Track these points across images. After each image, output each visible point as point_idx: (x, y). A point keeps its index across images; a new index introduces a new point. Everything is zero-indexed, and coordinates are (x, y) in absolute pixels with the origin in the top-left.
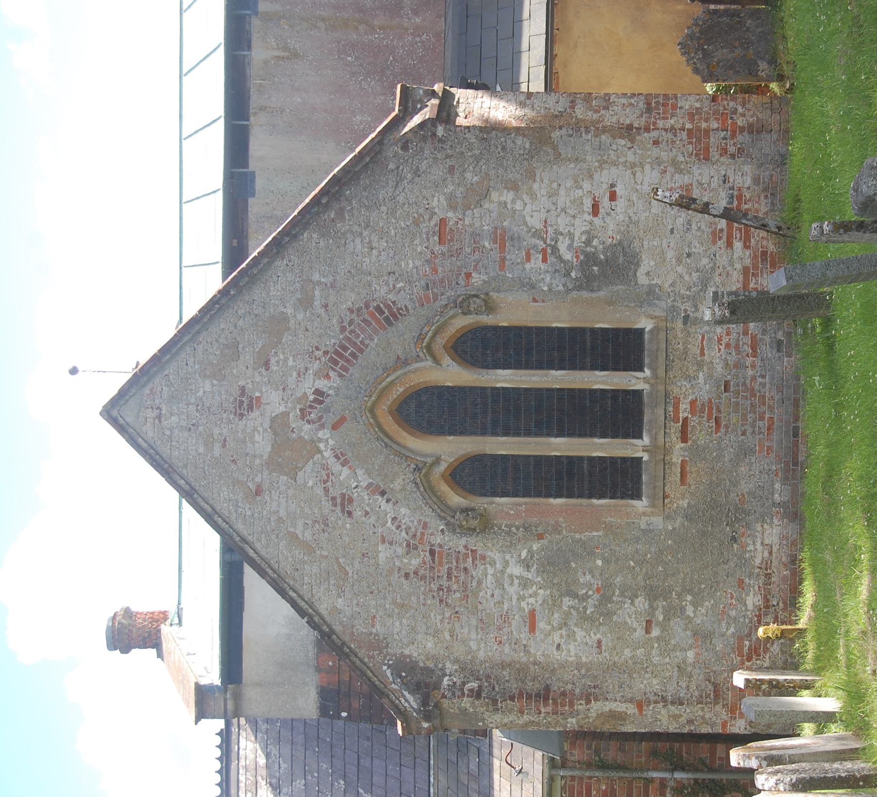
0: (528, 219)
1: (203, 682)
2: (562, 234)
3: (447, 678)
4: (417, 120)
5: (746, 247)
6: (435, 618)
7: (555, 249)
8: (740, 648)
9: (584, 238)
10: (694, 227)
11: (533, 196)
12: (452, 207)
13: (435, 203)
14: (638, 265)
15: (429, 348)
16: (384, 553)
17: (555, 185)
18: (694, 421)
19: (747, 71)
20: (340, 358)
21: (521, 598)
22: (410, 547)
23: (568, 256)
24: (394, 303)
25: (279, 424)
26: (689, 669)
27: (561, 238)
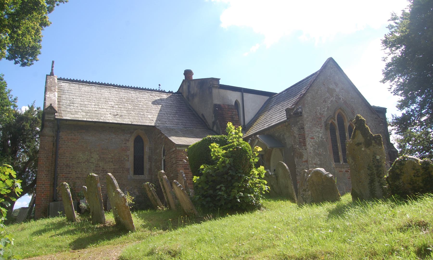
6: (310, 118)
16: (319, 108)
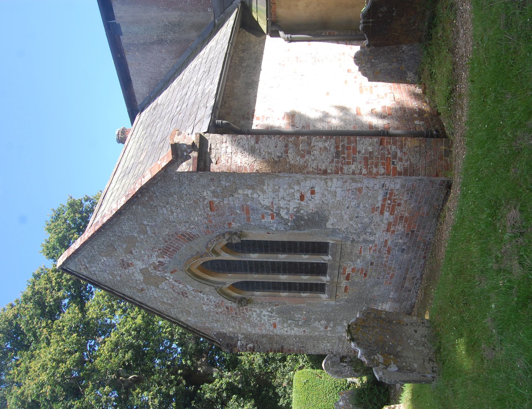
0: (262, 201)
2: (282, 208)
3: (239, 342)
5: (391, 214)
7: (278, 214)
9: (295, 210)
10: (361, 205)
11: (264, 192)
13: (205, 194)
14: (327, 221)
17: (277, 187)
19: (399, 77)
23: (286, 217)
24: (191, 233)
26: (343, 339)
27: (282, 210)
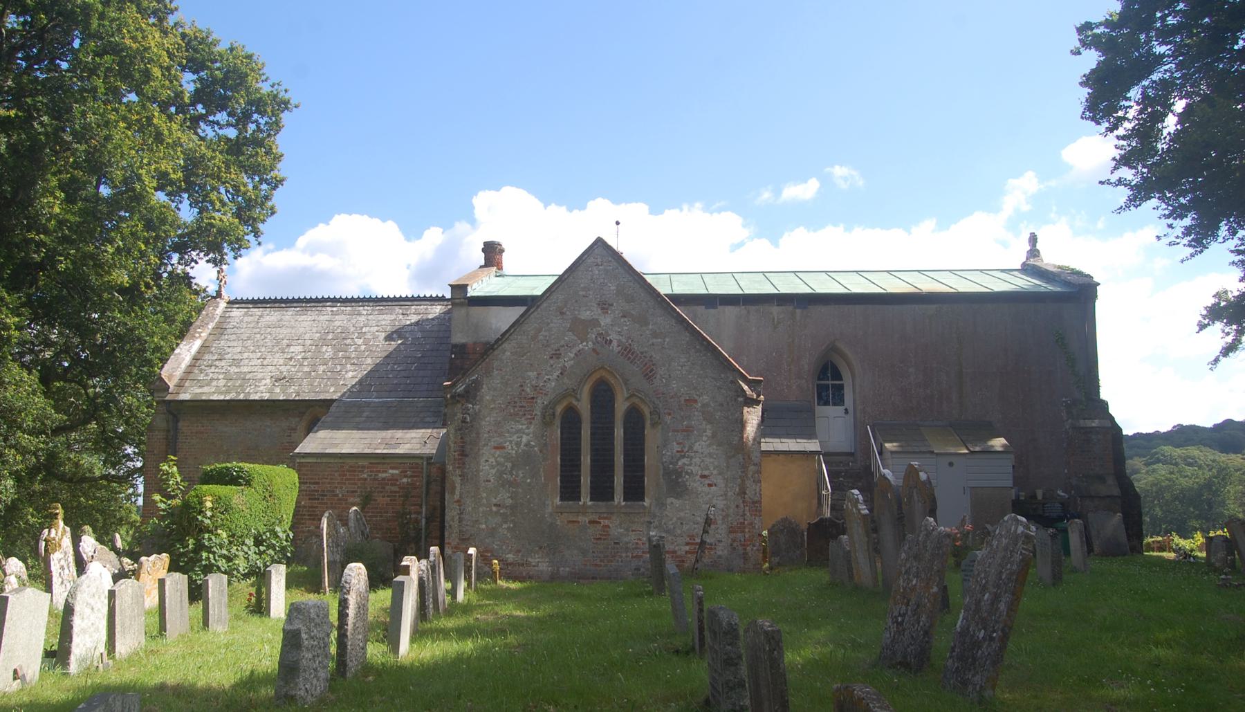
1: (469, 289)
4: (746, 388)
7: (684, 457)
8: (487, 551)
12: (703, 406)
15: (632, 395)
16: (533, 374)
18: (599, 527)
20: (627, 351)
21: (511, 442)
22: (535, 388)
25: (594, 323)
